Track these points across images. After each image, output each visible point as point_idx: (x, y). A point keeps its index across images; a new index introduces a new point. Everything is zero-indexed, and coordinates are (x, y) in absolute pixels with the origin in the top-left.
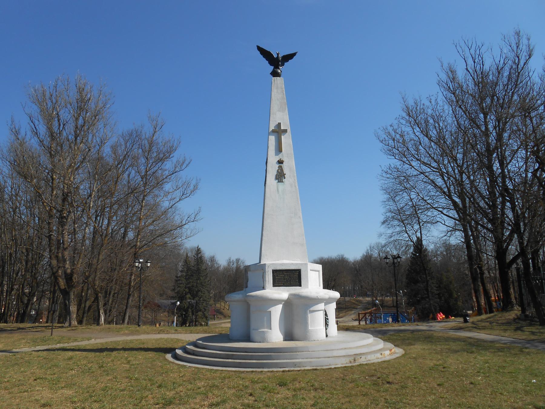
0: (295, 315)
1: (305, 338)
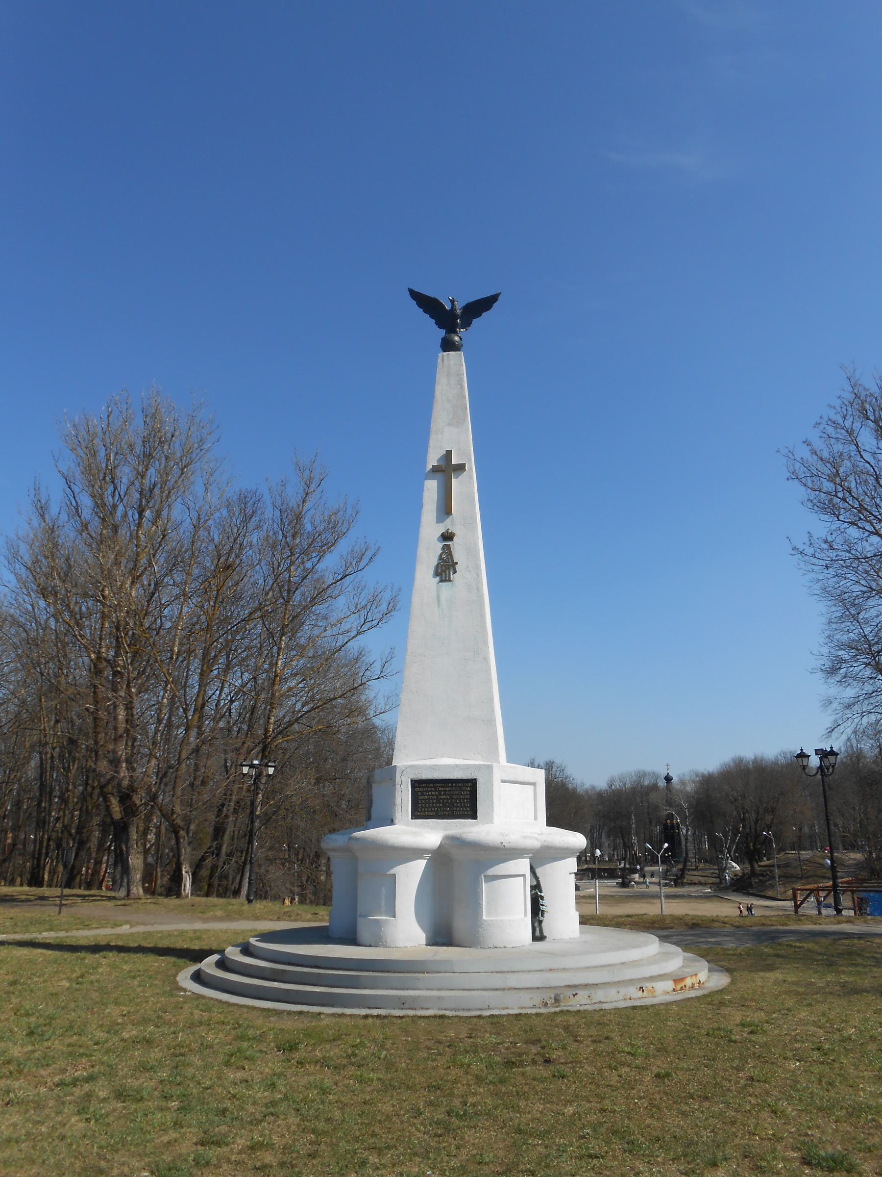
0: (455, 881)
1: (473, 941)
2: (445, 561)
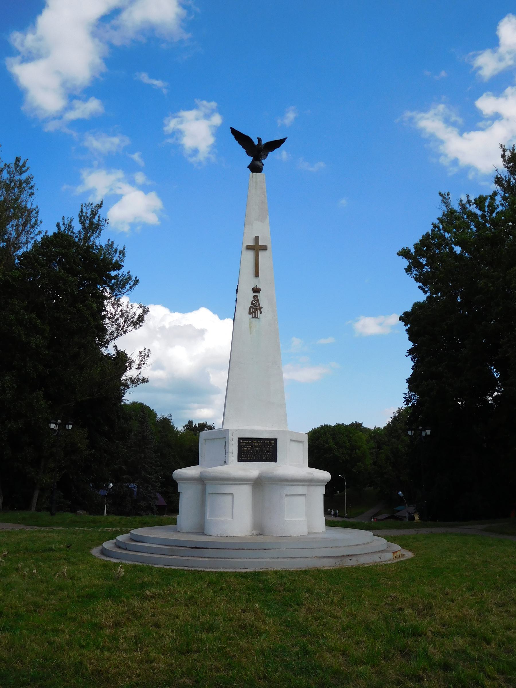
2: (254, 306)
